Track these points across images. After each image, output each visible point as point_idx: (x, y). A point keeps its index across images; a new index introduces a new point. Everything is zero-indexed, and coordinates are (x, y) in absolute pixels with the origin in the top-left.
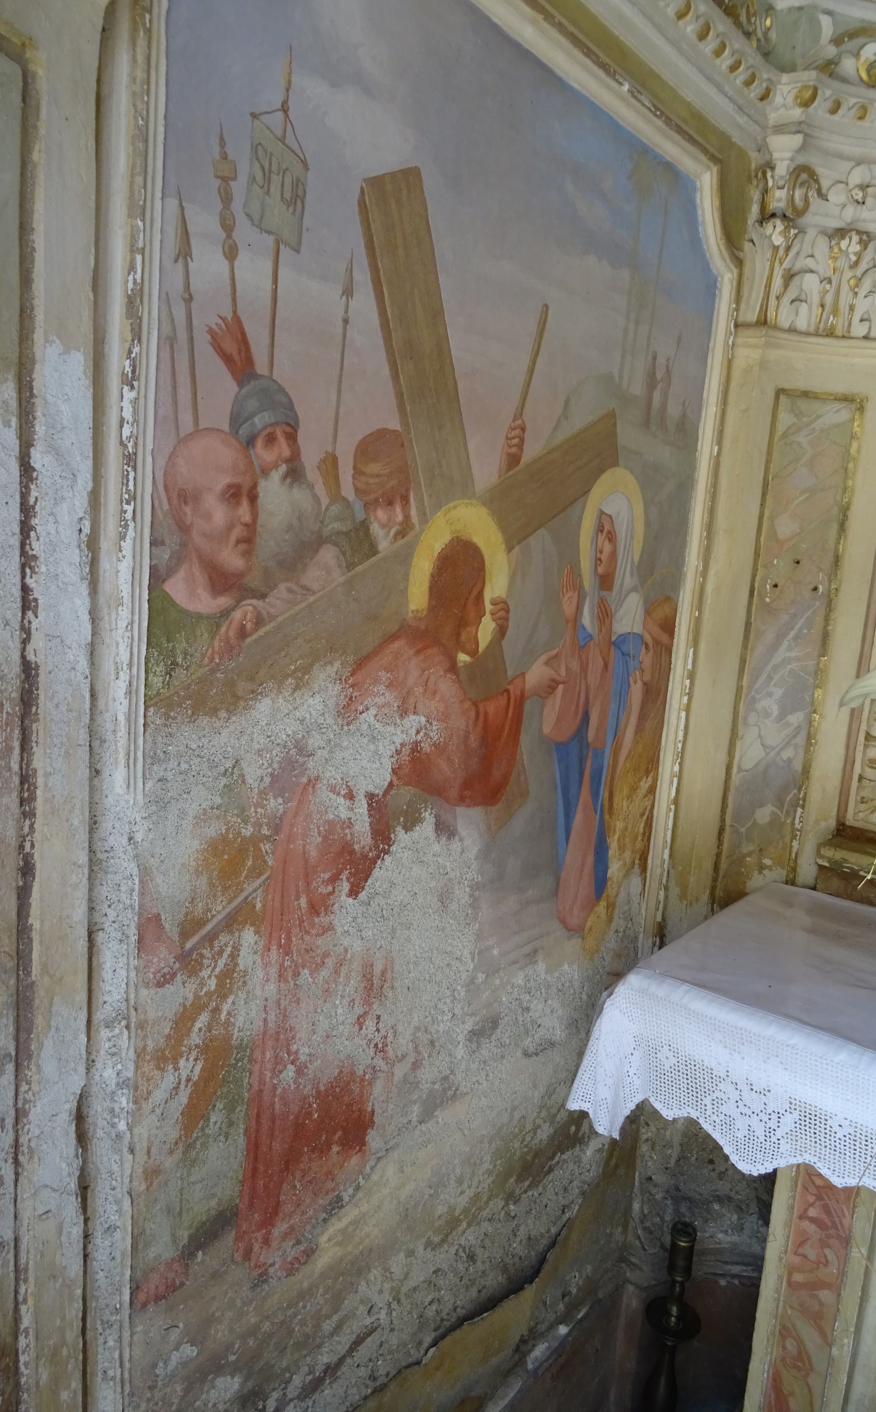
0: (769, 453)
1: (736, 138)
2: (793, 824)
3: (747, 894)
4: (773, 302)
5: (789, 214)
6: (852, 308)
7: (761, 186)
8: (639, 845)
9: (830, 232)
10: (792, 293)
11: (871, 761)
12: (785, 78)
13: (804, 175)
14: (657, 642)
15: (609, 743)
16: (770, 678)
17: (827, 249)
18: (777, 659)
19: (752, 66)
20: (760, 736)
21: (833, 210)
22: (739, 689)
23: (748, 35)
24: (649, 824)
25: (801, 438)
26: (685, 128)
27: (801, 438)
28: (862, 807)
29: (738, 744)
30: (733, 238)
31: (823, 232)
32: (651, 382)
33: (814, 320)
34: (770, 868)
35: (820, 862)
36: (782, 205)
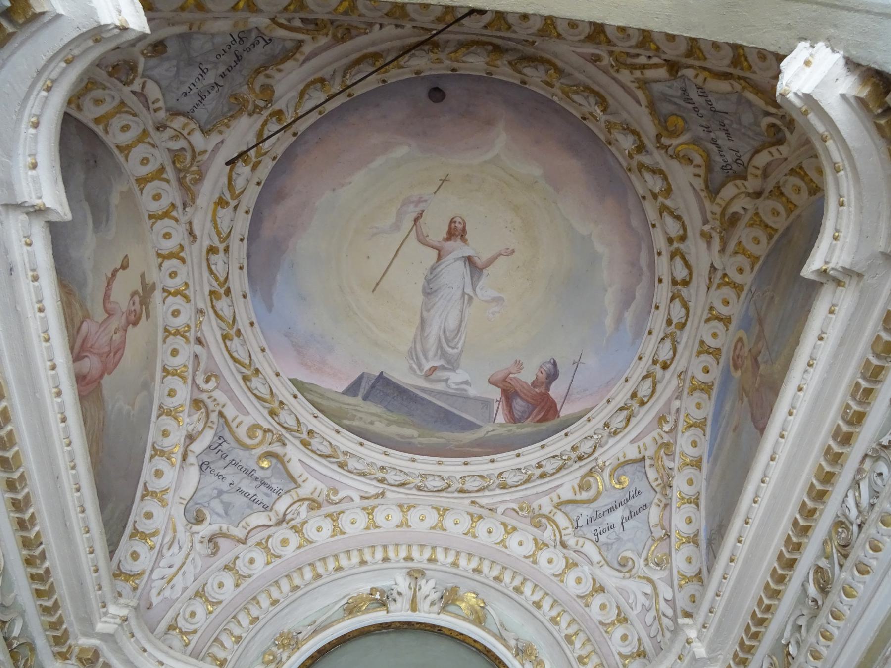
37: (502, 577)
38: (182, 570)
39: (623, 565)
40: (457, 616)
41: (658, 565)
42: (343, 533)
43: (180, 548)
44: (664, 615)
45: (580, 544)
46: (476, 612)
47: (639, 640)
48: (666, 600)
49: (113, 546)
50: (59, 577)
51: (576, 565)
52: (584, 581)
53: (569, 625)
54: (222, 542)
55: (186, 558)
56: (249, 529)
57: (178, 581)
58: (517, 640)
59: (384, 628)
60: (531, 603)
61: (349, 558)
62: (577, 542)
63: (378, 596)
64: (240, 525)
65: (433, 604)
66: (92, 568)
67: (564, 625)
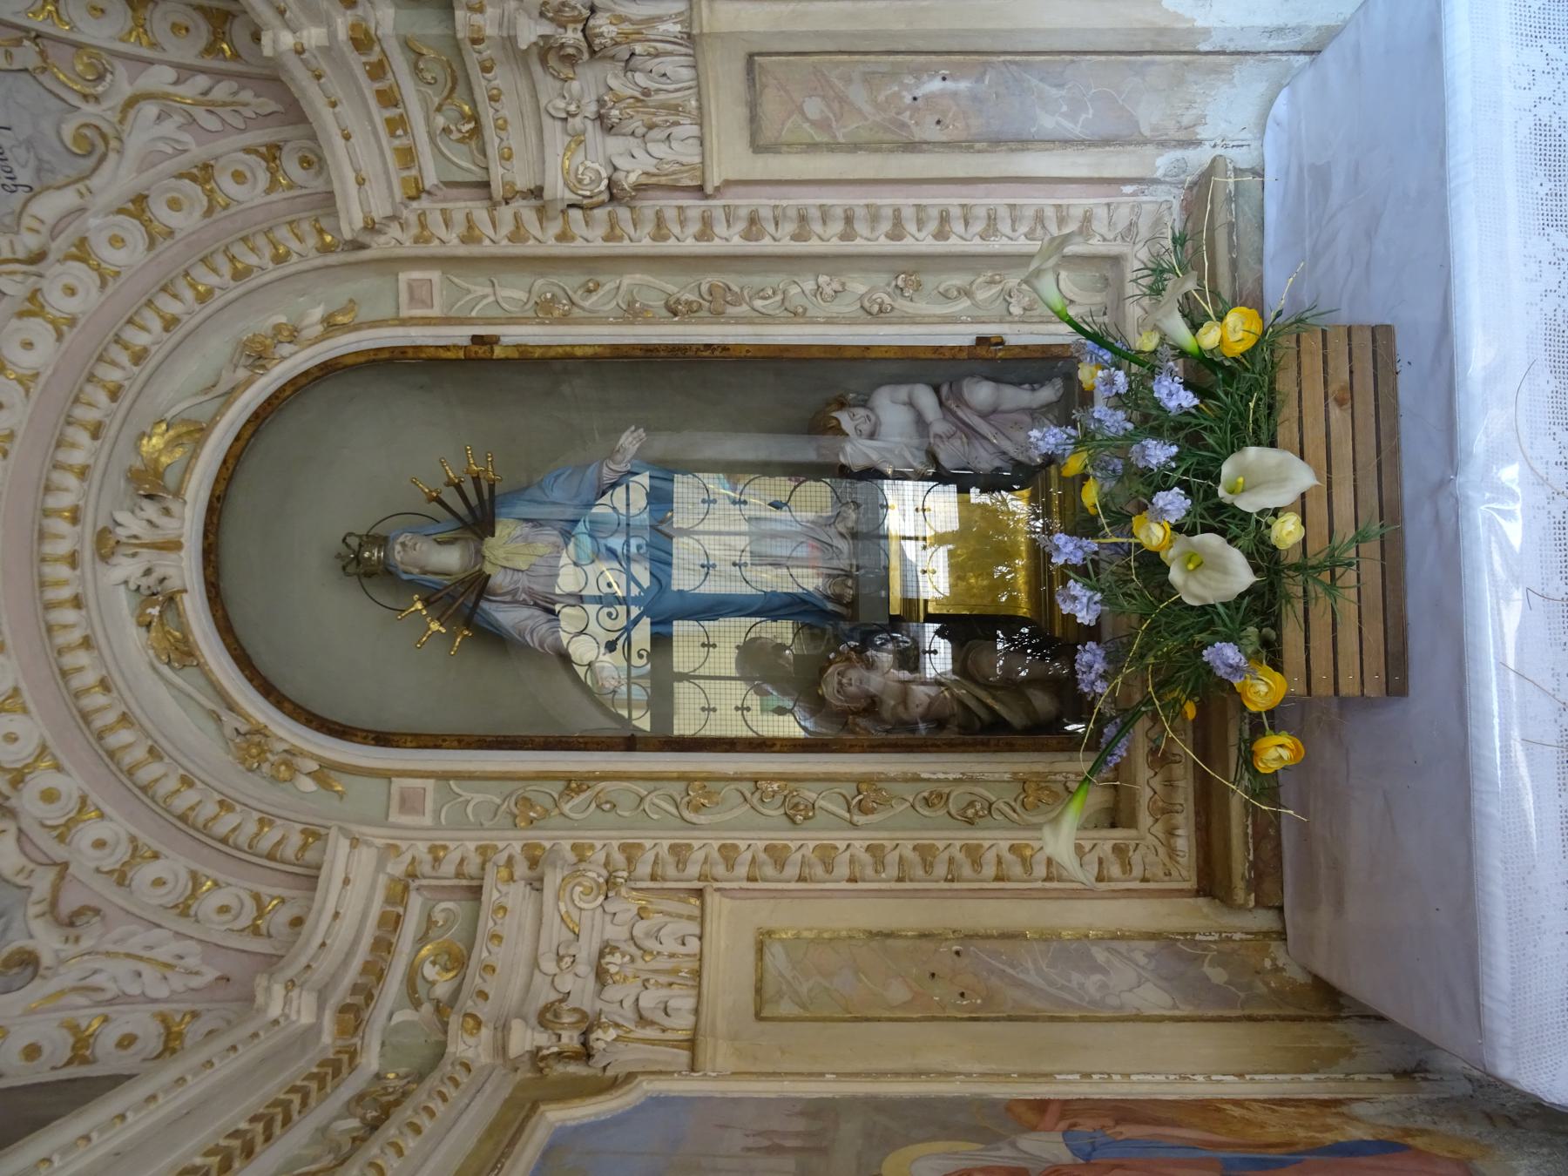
0: (824, 1020)
1: (505, 1093)
2: (1215, 942)
3: (1316, 978)
4: (669, 1036)
5: (584, 1027)
6: (672, 956)
7: (551, 1062)
8: (1313, 1110)
9: (598, 987)
10: (659, 1017)
11: (1124, 872)
12: (451, 1049)
13: (547, 1017)
14: (1062, 1117)
15: (1204, 1154)
16: (1062, 988)
17: (617, 987)
18: (1040, 983)
19: (442, 1081)
20: (1130, 990)
21: (579, 986)
22: (1083, 1019)
23: (405, 1094)
24: (1282, 1102)
25: (804, 989)
26: (506, 1141)
27: (804, 989)
28: (1175, 873)
29: (1147, 1013)
30: (614, 1084)
31: (599, 993)
32: (775, 1150)
33: (685, 992)
34: (1274, 960)
35: (1252, 904)
36: (576, 1034)
37: (111, 385)
38: (146, 954)
39: (95, 148)
40: (187, 469)
41: (100, 78)
42: (16, 691)
43: (95, 972)
44: (205, 93)
45: (35, 225)
46: (179, 436)
47: (247, 151)
48: (176, 83)
49: (115, 1081)
50: (255, 1101)
51: (82, 242)
52: (117, 231)
53: (215, 271)
54: (68, 904)
55: (116, 955)
56: (31, 866)
57: (164, 953)
58: (236, 367)
59: (218, 594)
60: (166, 336)
61: (80, 669)
62: (31, 230)
63: (155, 611)
64: (26, 883)
65: (167, 512)
66: (232, 1055)
67: (213, 280)
